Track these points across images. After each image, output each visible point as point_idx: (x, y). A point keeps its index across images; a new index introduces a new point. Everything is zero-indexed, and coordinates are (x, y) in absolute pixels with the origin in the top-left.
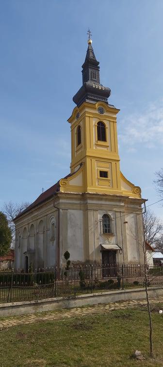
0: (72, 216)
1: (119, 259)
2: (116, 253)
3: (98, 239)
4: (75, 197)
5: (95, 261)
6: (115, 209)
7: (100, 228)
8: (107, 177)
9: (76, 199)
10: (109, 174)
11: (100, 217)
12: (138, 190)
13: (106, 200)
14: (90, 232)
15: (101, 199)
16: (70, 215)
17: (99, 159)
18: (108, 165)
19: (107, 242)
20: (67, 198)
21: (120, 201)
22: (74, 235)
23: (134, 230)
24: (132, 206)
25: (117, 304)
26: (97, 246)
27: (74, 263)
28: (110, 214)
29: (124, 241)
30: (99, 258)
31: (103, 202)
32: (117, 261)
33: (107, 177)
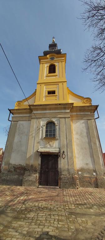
0: (21, 126)
1: (62, 164)
2: (58, 158)
3: (38, 143)
4: (25, 111)
5: (32, 166)
6: (59, 116)
7: (42, 133)
8: (55, 94)
9: (26, 113)
10: (56, 92)
11: (43, 123)
12: (89, 99)
13: (50, 109)
14: (30, 137)
15: (45, 109)
16: (19, 125)
17: (47, 84)
18: (55, 86)
19: (49, 146)
20: (19, 113)
21: (65, 108)
22: (20, 141)
23: (85, 134)
24: (82, 113)
25: (91, 229)
26: (35, 150)
27: (15, 166)
28: (54, 120)
29: (69, 144)
30: (37, 162)
31: (48, 112)
32: (59, 167)
33: (55, 94)
